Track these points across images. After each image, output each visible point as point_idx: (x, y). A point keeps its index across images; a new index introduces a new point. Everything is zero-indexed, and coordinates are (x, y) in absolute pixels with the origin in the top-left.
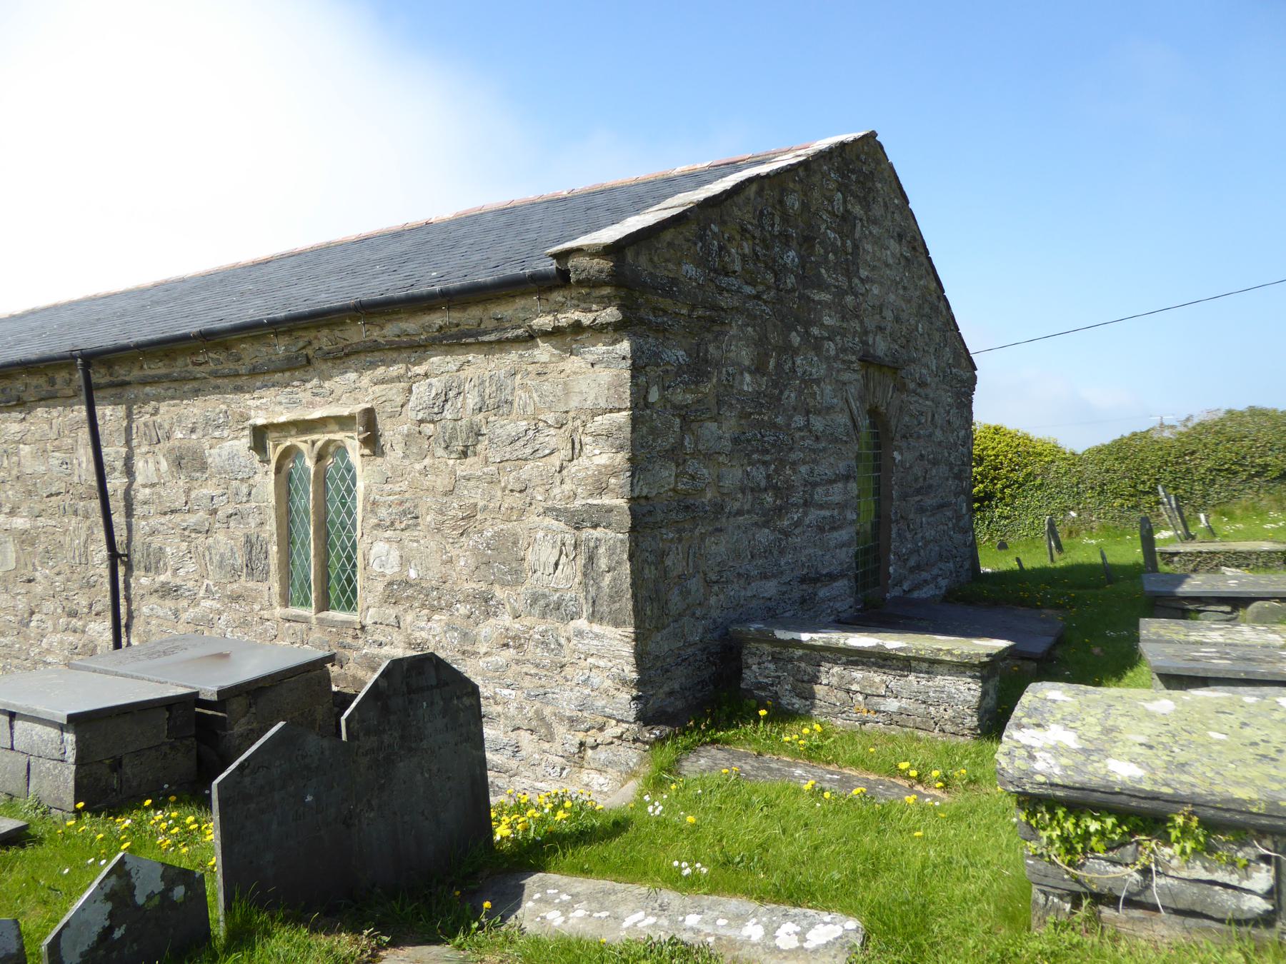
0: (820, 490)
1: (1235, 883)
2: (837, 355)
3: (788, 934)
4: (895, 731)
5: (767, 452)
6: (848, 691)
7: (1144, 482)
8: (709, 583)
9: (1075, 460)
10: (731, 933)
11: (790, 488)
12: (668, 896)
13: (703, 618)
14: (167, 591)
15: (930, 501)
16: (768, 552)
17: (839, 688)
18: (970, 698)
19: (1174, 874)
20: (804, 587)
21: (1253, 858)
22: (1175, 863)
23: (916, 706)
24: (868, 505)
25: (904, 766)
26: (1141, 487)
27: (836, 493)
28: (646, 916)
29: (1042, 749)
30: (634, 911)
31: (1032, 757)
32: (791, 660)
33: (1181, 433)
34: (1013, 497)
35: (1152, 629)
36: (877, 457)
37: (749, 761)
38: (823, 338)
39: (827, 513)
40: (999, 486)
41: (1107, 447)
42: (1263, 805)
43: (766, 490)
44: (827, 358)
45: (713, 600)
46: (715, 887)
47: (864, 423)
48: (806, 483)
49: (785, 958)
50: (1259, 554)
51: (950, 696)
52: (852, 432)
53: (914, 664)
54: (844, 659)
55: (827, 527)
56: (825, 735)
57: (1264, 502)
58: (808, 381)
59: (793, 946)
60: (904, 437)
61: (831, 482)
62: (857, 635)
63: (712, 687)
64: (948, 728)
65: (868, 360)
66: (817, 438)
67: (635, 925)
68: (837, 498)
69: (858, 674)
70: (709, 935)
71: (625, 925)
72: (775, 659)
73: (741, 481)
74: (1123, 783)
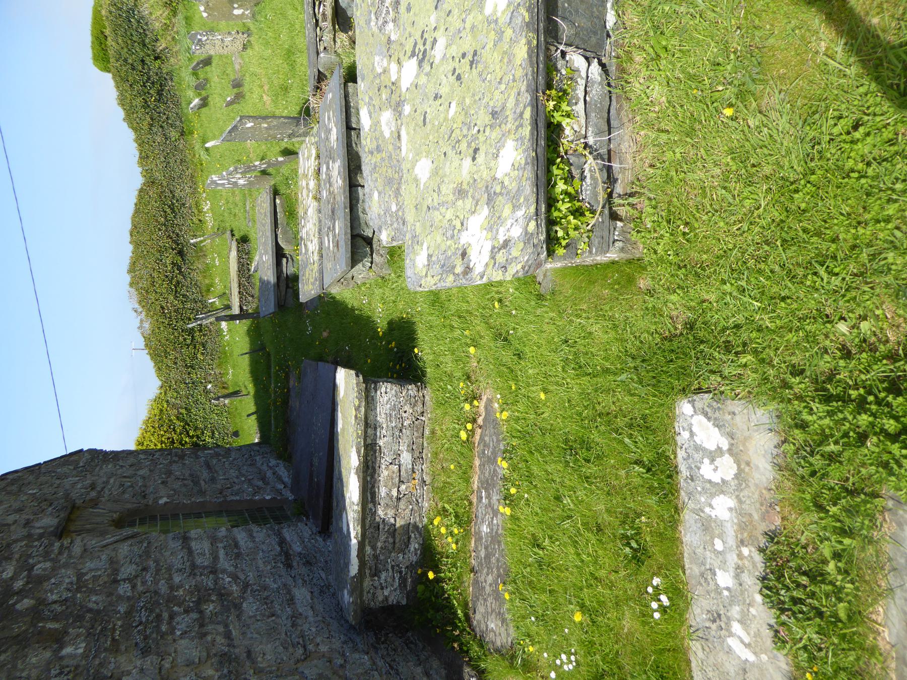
0: (199, 561)
1: (584, 82)
2: (52, 560)
3: (716, 469)
4: (427, 454)
5: (159, 617)
6: (398, 499)
7: (185, 340)
8: (307, 656)
9: (166, 386)
10: (730, 531)
11: (197, 588)
12: (698, 615)
13: (343, 655)
16: (266, 601)
17: (396, 508)
18: (393, 392)
19: (584, 129)
20: (295, 564)
21: (564, 62)
22: (576, 128)
23: (405, 438)
24: (209, 523)
25: (463, 435)
26: (189, 342)
27: (200, 546)
28: (731, 635)
29: (495, 238)
30: (730, 651)
31: (506, 244)
32: (376, 557)
33: (147, 315)
34: (196, 428)
35: (307, 290)
36: (164, 518)
37: (482, 579)
38: (29, 576)
39: (222, 553)
40: (187, 440)
41: (156, 364)
42: (530, 34)
43: (201, 612)
44: (54, 569)
45: (324, 648)
46: (673, 563)
47: (128, 531)
48: (193, 574)
49: (748, 464)
50: (239, 258)
51: (393, 408)
52: (138, 539)
53: (369, 441)
54: (370, 505)
55: (236, 551)
56: (444, 512)
57: (200, 266)
58: (80, 584)
59: (731, 460)
60: (144, 497)
61: (190, 552)
62: (347, 495)
63: (410, 634)
64: (419, 408)
65: (61, 532)
66: (145, 569)
67: (747, 646)
68: (206, 545)
69: (383, 491)
70: (740, 556)
71: (752, 658)
72: (376, 573)
73: (192, 639)
74: (524, 151)
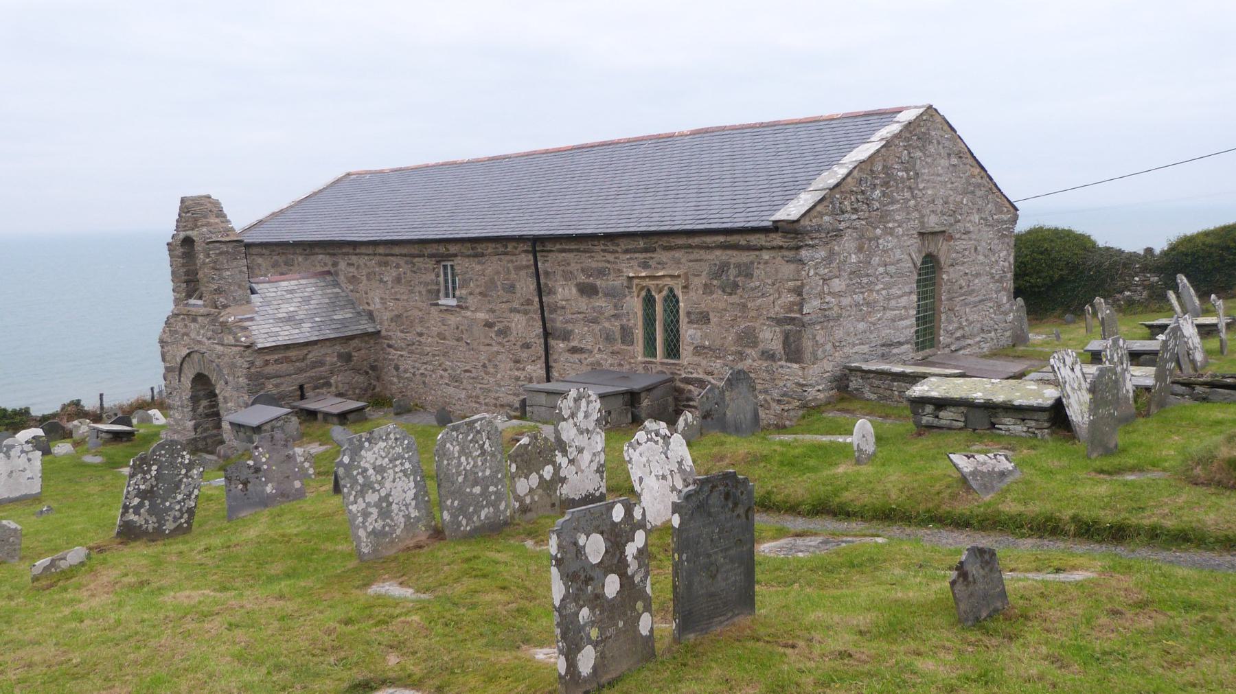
14: (574, 350)
15: (971, 299)
27: (904, 301)
